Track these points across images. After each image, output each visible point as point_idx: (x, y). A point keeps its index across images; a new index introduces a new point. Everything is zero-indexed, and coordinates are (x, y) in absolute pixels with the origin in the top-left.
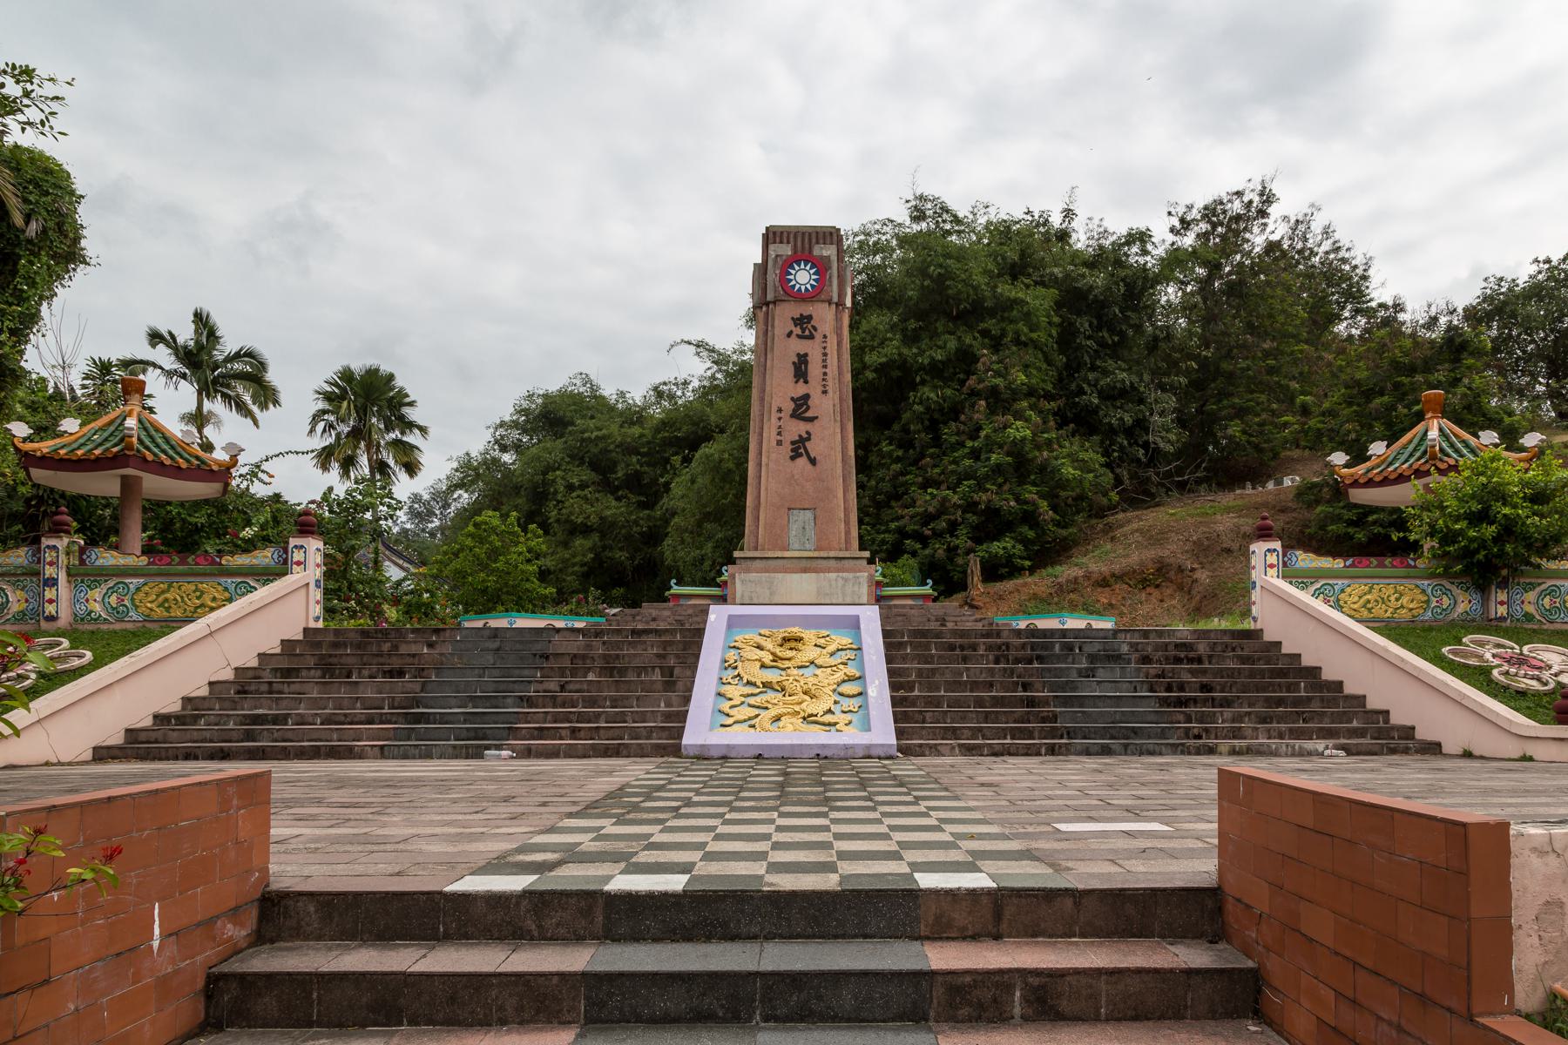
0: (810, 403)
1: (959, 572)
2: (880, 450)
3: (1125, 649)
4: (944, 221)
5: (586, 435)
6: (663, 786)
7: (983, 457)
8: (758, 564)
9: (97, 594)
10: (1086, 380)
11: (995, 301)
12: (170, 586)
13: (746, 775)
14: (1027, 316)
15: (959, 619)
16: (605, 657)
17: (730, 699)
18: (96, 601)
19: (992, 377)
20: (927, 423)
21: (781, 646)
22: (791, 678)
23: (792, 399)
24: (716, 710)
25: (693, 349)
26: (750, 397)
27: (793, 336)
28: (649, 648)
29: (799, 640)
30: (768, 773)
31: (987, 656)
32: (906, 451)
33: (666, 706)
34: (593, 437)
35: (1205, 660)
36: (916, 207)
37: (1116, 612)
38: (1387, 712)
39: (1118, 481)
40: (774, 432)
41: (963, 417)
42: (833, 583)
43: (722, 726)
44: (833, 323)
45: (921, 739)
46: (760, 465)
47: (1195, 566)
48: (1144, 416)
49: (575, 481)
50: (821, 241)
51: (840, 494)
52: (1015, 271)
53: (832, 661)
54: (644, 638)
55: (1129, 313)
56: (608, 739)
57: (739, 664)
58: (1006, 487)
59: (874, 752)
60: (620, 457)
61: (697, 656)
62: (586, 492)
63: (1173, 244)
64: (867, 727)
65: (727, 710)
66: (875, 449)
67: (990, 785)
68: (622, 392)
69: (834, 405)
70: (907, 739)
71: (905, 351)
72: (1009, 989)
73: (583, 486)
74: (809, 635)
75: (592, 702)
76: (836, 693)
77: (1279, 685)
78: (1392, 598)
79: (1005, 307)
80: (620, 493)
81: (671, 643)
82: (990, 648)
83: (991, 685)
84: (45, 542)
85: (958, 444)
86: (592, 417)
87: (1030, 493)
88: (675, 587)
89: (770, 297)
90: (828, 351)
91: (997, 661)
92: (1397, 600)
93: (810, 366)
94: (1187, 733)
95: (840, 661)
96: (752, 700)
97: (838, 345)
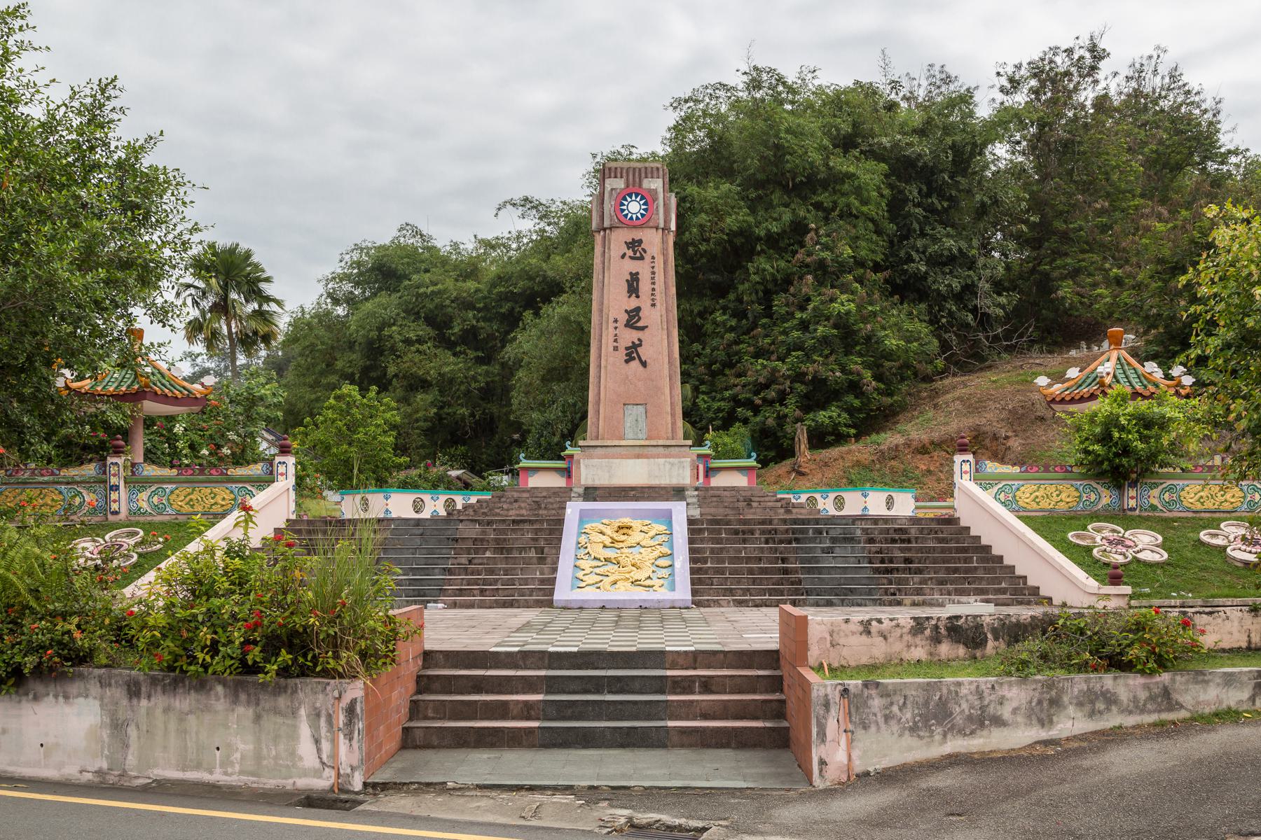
3: (859, 533)
5: (422, 290)
7: (812, 327)
9: (144, 495)
10: (914, 247)
12: (193, 490)
14: (858, 191)
15: (762, 499)
16: (497, 541)
18: (144, 500)
19: (822, 250)
20: (761, 294)
23: (626, 311)
27: (627, 257)
29: (629, 528)
30: (609, 616)
35: (913, 540)
37: (934, 478)
38: (1026, 577)
39: (945, 346)
40: (611, 339)
41: (792, 290)
42: (662, 467)
44: (660, 245)
46: (600, 366)
47: (1010, 434)
48: (973, 282)
49: (412, 335)
50: (649, 175)
51: (667, 391)
52: (846, 143)
53: (652, 543)
55: (959, 179)
57: (588, 545)
58: (832, 358)
60: (456, 311)
61: (560, 540)
63: (1002, 103)
64: (673, 589)
65: (581, 577)
68: (455, 243)
72: (694, 682)
73: (420, 341)
74: (636, 524)
75: (491, 572)
77: (959, 558)
78: (1054, 495)
79: (835, 180)
80: (458, 349)
81: (541, 530)
83: (760, 559)
84: (110, 460)
86: (427, 271)
87: (855, 364)
88: (524, 461)
89: (607, 224)
91: (767, 543)
92: (1058, 495)
93: (640, 283)
94: (886, 592)
96: (597, 571)
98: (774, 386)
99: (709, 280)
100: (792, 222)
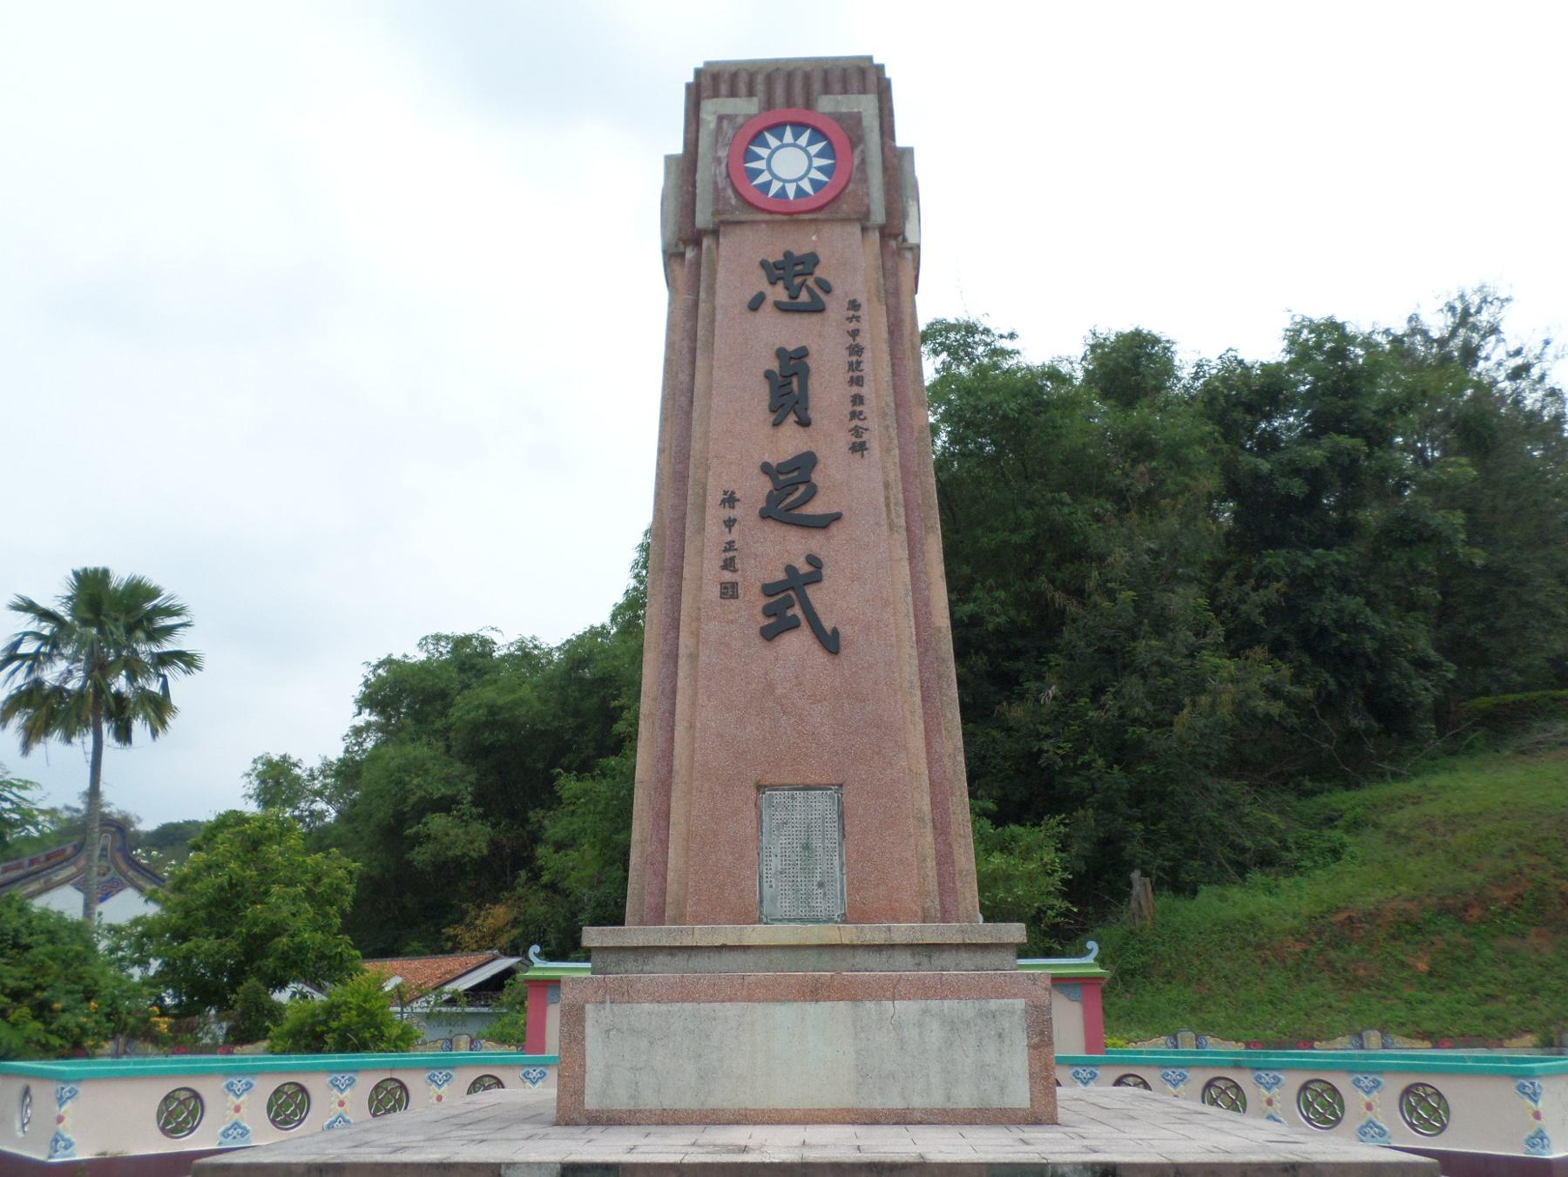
0: (816, 477)
8: (662, 972)
23: (766, 469)
27: (767, 307)
40: (713, 560)
46: (673, 657)
69: (887, 486)
90: (864, 340)
97: (891, 332)
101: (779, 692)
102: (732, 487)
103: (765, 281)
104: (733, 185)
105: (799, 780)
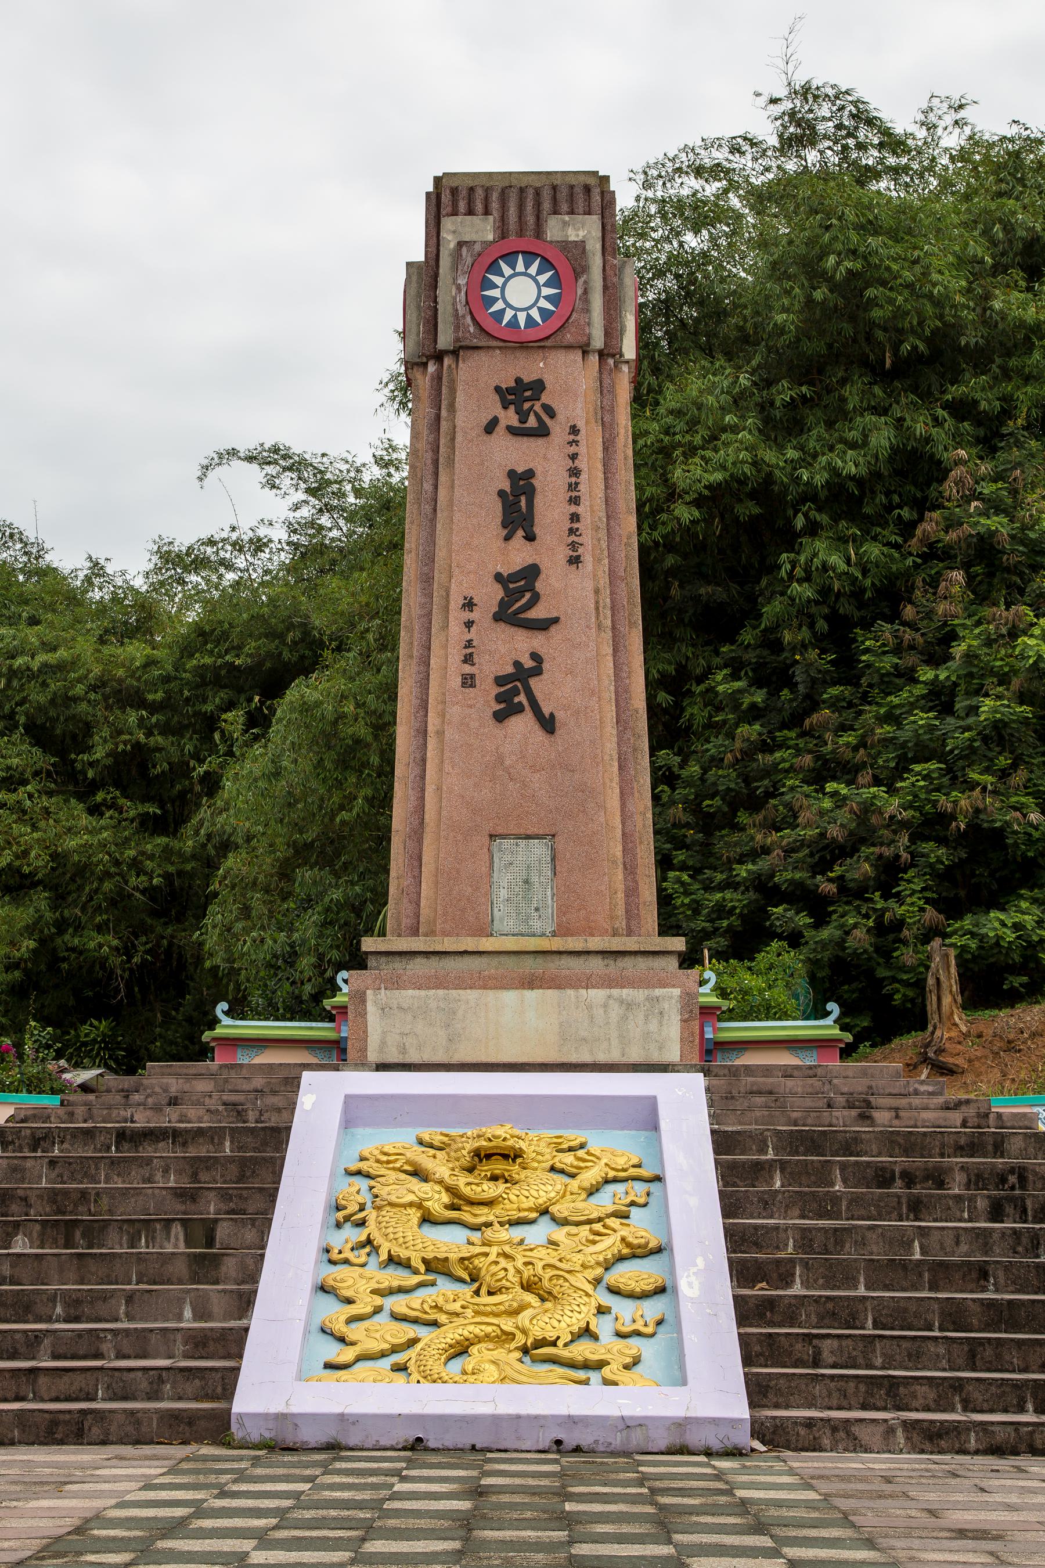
0: (539, 586)
1: (907, 984)
2: (711, 690)
4: (861, 147)
5: (19, 661)
6: (183, 1521)
7: (960, 704)
8: (419, 966)
11: (985, 331)
13: (384, 1493)
15: (903, 1102)
16: (53, 1197)
17: (349, 1301)
20: (822, 625)
21: (470, 1170)
22: (494, 1250)
23: (498, 577)
24: (317, 1323)
25: (255, 473)
26: (398, 571)
27: (500, 429)
28: (158, 1176)
29: (512, 1155)
31: (972, 1199)
32: (774, 693)
33: (198, 1316)
34: (35, 665)
36: (792, 114)
40: (456, 655)
41: (909, 612)
43: (328, 1366)
44: (594, 397)
45: (810, 1406)
46: (423, 732)
50: (565, 207)
51: (613, 801)
54: (147, 1151)
56: (57, 1399)
57: (371, 1214)
58: (1019, 777)
59: (696, 1438)
61: (272, 1196)
62: (21, 793)
65: (340, 1327)
66: (699, 689)
67: (981, 1535)
69: (597, 591)
70: (777, 1406)
71: (769, 456)
76: (601, 1288)
80: (100, 797)
81: (208, 1163)
82: (977, 1180)
83: (982, 1274)
85: (899, 675)
86: (33, 621)
88: (226, 1021)
89: (445, 341)
90: (582, 463)
91: (996, 1213)
93: (538, 501)
95: (611, 1208)
96: (399, 1304)
97: (606, 449)
98: (866, 850)
99: (697, 599)
100: (895, 451)
101: (508, 763)
102: (470, 593)
103: (499, 405)
104: (471, 313)
105: (522, 831)
